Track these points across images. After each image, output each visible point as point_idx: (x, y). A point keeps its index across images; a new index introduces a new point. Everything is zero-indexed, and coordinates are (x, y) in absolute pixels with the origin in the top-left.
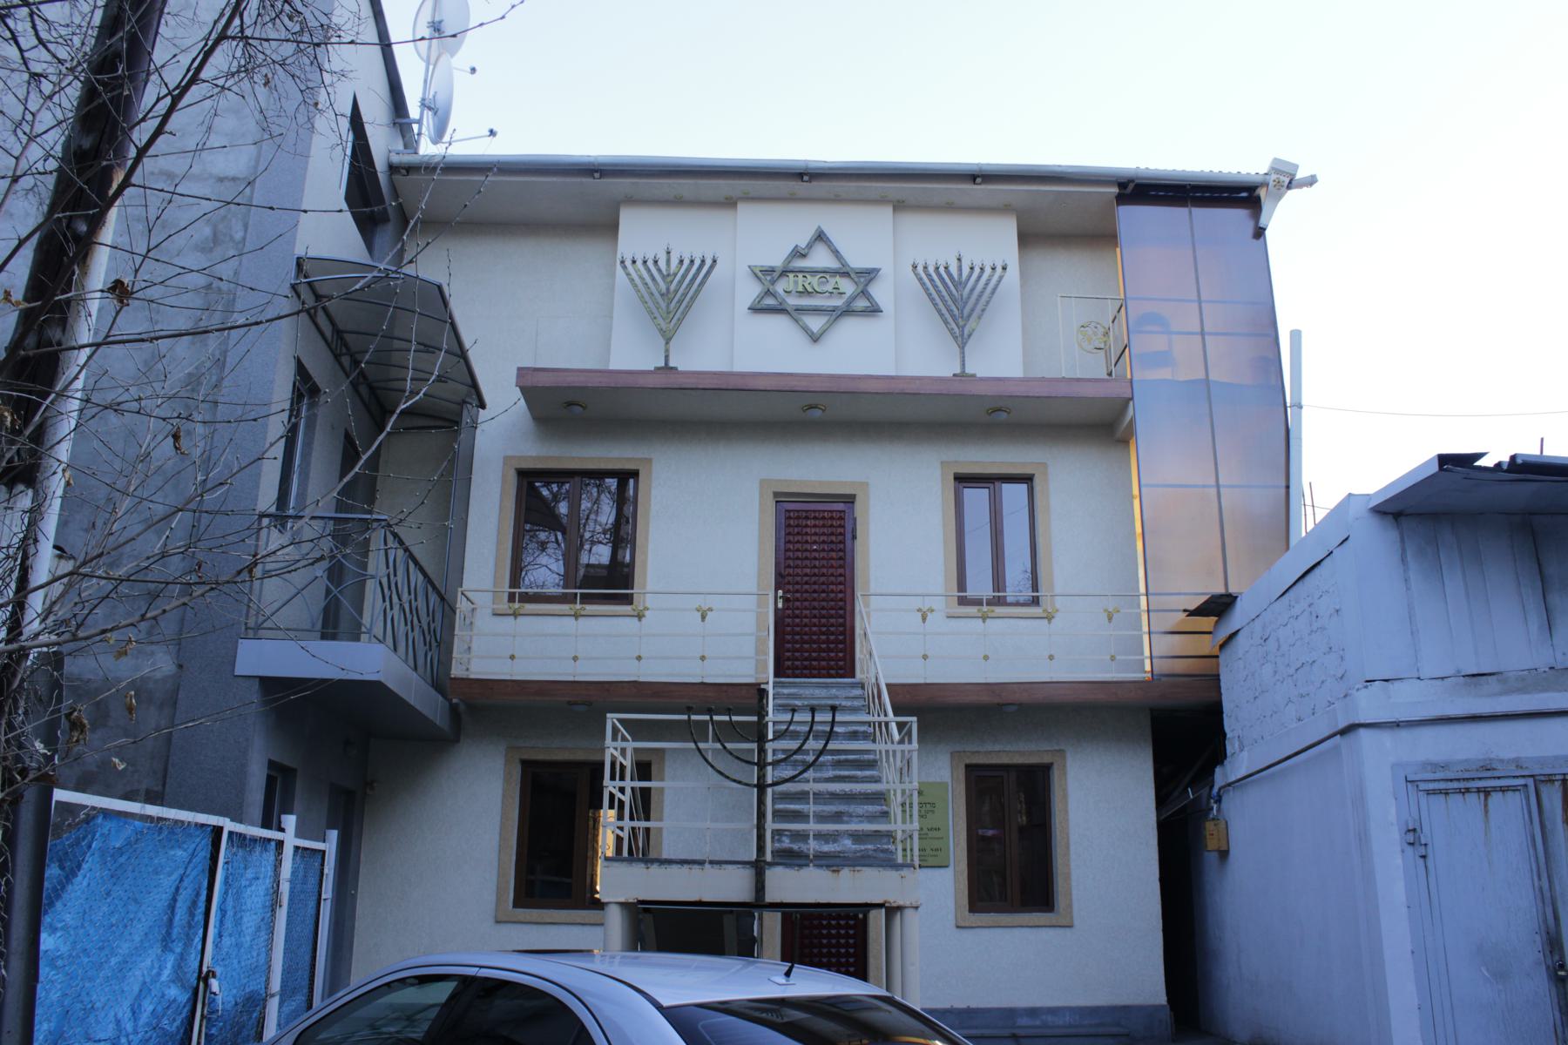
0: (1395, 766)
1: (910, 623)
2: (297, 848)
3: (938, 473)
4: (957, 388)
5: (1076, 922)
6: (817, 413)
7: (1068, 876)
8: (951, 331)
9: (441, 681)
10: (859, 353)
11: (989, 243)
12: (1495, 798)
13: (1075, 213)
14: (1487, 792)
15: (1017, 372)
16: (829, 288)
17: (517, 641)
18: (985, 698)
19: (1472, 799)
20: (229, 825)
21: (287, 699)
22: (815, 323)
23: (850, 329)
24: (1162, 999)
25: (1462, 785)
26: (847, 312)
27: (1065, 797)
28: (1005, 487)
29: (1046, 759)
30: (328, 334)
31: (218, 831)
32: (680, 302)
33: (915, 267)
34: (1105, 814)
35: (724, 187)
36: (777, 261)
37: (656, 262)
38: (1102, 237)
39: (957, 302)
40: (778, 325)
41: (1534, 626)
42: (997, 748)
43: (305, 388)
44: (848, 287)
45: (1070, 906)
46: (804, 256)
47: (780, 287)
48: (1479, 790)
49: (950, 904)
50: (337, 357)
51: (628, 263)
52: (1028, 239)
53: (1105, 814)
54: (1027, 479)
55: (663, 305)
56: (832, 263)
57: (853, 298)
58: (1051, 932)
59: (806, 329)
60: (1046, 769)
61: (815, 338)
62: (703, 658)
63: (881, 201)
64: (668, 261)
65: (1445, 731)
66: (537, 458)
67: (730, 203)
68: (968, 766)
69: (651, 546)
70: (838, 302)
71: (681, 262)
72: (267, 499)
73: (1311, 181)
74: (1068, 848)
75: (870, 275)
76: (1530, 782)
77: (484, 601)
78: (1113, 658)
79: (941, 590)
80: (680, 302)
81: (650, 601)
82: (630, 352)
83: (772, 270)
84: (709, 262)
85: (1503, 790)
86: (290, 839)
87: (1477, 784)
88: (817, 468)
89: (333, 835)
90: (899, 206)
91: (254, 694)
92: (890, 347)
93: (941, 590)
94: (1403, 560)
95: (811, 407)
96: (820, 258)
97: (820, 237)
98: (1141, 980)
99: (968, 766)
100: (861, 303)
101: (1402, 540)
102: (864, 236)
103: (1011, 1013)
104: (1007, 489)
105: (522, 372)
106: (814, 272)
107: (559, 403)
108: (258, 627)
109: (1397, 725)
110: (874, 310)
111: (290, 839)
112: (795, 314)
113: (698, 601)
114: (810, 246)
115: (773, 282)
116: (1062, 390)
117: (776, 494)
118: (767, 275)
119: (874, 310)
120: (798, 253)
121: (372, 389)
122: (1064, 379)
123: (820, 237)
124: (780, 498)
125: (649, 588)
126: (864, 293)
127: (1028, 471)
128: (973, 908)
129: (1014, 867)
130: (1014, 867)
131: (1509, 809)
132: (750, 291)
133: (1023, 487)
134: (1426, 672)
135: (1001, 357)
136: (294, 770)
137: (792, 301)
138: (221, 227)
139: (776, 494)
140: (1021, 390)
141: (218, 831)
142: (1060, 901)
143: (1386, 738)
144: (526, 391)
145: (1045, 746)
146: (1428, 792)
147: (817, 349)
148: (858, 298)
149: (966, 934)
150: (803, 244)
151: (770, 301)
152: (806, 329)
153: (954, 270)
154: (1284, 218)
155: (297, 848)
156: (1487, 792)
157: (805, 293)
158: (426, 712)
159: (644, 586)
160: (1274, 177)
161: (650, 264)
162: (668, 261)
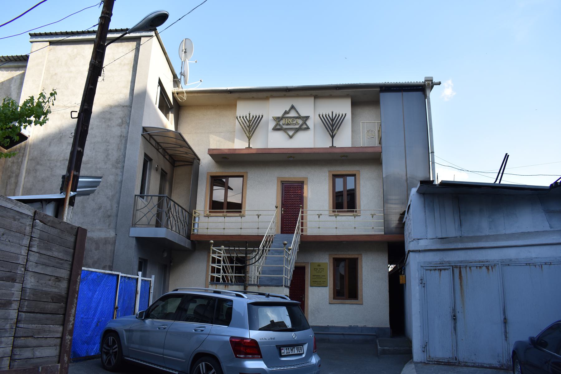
3: (328, 174)
4: (330, 151)
5: (364, 303)
6: (291, 159)
7: (362, 290)
8: (330, 134)
9: (188, 236)
11: (343, 108)
12: (443, 272)
13: (365, 97)
14: (440, 270)
15: (350, 145)
16: (295, 122)
17: (209, 224)
19: (437, 272)
20: (121, 274)
21: (142, 242)
22: (291, 133)
24: (388, 325)
25: (435, 268)
26: (297, 130)
28: (348, 178)
29: (356, 256)
31: (118, 275)
32: (253, 128)
33: (319, 115)
35: (265, 94)
36: (280, 115)
37: (246, 117)
39: (332, 125)
41: (457, 226)
42: (343, 253)
43: (147, 160)
44: (300, 122)
45: (362, 299)
46: (288, 113)
47: (281, 123)
48: (439, 269)
49: (328, 297)
50: (158, 150)
51: (238, 118)
52: (354, 104)
53: (373, 274)
54: (354, 175)
55: (248, 129)
56: (296, 115)
57: (302, 125)
59: (288, 135)
60: (357, 259)
61: (291, 137)
63: (310, 96)
65: (431, 254)
66: (216, 172)
67: (267, 98)
68: (334, 258)
69: (247, 197)
70: (297, 127)
71: (253, 117)
72: (138, 192)
73: (439, 84)
74: (362, 281)
75: (307, 118)
76: (451, 267)
77: (202, 213)
78: (373, 228)
79: (327, 209)
80: (253, 128)
81: (247, 213)
82: (239, 144)
83: (279, 118)
84: (261, 117)
85: (445, 269)
86: (140, 278)
87: (439, 268)
88: (293, 174)
91: (134, 242)
92: (310, 140)
93: (327, 209)
94: (425, 207)
96: (293, 114)
97: (293, 107)
99: (334, 258)
100: (305, 126)
102: (305, 107)
103: (327, 328)
105: (209, 150)
106: (290, 118)
108: (135, 224)
109: (419, 251)
110: (308, 128)
111: (140, 278)
112: (285, 130)
113: (257, 213)
114: (290, 110)
115: (279, 121)
117: (281, 181)
118: (278, 119)
119: (308, 128)
120: (286, 112)
122: (361, 147)
123: (293, 107)
125: (246, 209)
127: (354, 173)
128: (334, 298)
129: (347, 288)
130: (347, 288)
132: (272, 125)
133: (353, 178)
135: (344, 140)
136: (147, 260)
137: (285, 127)
139: (281, 181)
140: (349, 151)
142: (359, 297)
143: (417, 255)
144: (211, 155)
146: (427, 270)
147: (292, 140)
148: (302, 125)
149: (333, 306)
150: (288, 110)
151: (278, 127)
152: (288, 135)
153: (331, 116)
154: (433, 95)
155: (142, 280)
156: (440, 270)
157: (288, 124)
158: (182, 244)
159: (245, 208)
160: (426, 83)
161: (244, 118)
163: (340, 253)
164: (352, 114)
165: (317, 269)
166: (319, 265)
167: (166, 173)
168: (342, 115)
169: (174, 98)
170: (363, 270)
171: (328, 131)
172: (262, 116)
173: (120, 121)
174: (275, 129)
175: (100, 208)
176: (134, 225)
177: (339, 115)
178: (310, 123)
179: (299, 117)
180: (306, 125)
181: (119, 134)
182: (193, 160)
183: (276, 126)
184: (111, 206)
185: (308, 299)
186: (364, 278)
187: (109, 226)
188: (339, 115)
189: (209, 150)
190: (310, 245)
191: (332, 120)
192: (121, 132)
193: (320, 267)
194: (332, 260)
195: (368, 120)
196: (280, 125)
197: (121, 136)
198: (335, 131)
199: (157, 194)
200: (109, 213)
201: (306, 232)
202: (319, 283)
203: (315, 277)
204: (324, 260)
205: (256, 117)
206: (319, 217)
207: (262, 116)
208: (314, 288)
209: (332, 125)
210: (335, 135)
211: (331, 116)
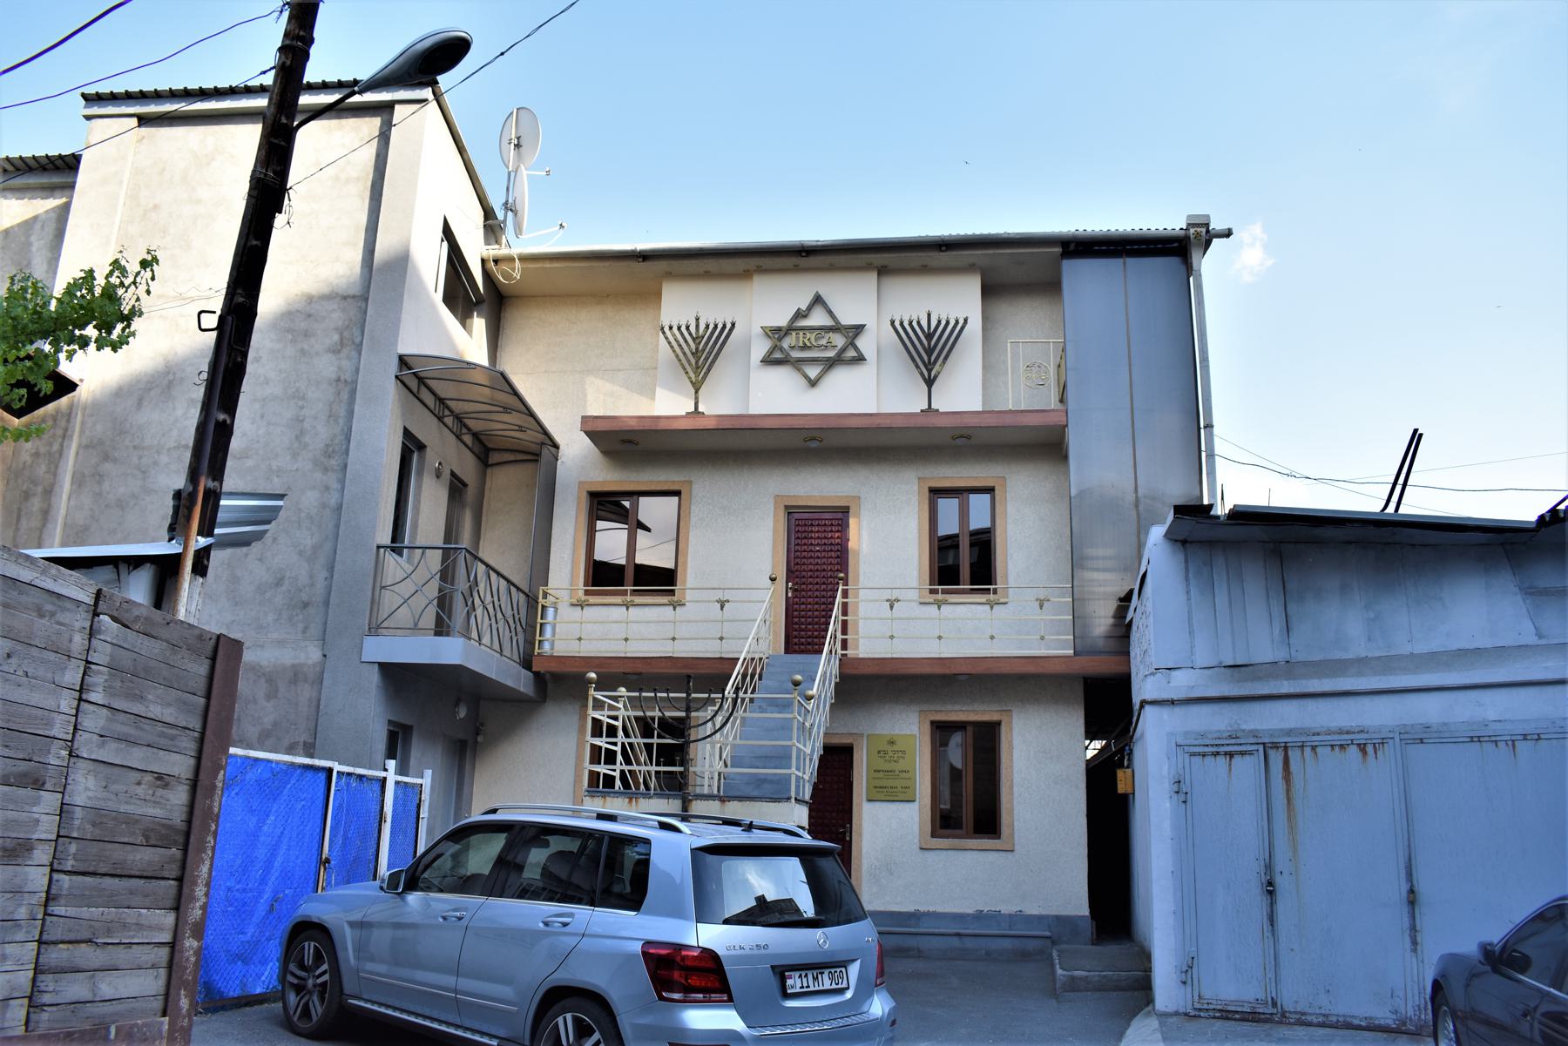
0: (1170, 734)
1: (892, 608)
2: (397, 783)
3: (916, 488)
5: (1017, 848)
6: (814, 444)
10: (850, 395)
11: (956, 300)
12: (1237, 759)
13: (1020, 270)
14: (1231, 755)
15: (977, 406)
16: (824, 342)
17: (583, 628)
19: (1221, 760)
21: (396, 676)
22: (813, 372)
23: (841, 378)
24: (1084, 910)
25: (1215, 749)
26: (830, 364)
31: (330, 770)
32: (707, 359)
33: (893, 323)
34: (1044, 760)
36: (783, 322)
37: (687, 328)
38: (1051, 287)
39: (928, 350)
40: (782, 374)
44: (839, 340)
45: (1012, 835)
46: (805, 316)
47: (786, 344)
48: (1226, 754)
50: (440, 419)
51: (666, 329)
52: (990, 291)
53: (1044, 760)
54: (990, 490)
55: (693, 361)
56: (829, 322)
57: (843, 350)
58: (995, 854)
59: (806, 377)
60: (999, 723)
61: (813, 383)
63: (867, 268)
64: (697, 326)
65: (1205, 709)
66: (604, 482)
68: (932, 723)
69: (690, 550)
70: (831, 354)
72: (385, 537)
73: (1228, 234)
75: (859, 329)
76: (1261, 748)
77: (564, 596)
78: (1042, 638)
79: (915, 584)
80: (707, 359)
81: (689, 595)
82: (669, 403)
83: (779, 329)
84: (729, 326)
85: (1242, 753)
86: (392, 777)
87: (1227, 750)
88: (818, 486)
89: (428, 773)
90: (883, 271)
92: (868, 391)
94: (1187, 579)
96: (818, 319)
97: (818, 300)
98: (1067, 890)
99: (932, 723)
100: (851, 353)
101: (1186, 561)
102: (854, 300)
104: (974, 499)
105: (585, 419)
107: (618, 441)
108: (378, 627)
109: (1173, 702)
110: (860, 359)
112: (797, 364)
113: (719, 595)
114: (810, 308)
115: (780, 339)
116: (1009, 421)
117: (786, 507)
118: (777, 334)
119: (860, 359)
120: (800, 315)
121: (475, 435)
122: (1010, 411)
123: (818, 300)
124: (790, 511)
126: (853, 344)
132: (760, 348)
134: (1199, 664)
135: (962, 392)
137: (796, 354)
139: (786, 507)
141: (330, 770)
142: (1005, 830)
143: (1165, 713)
144: (589, 434)
145: (995, 707)
146: (1193, 754)
147: (816, 392)
148: (844, 349)
149: (930, 855)
150: (804, 308)
151: (778, 355)
152: (806, 377)
153: (924, 323)
154: (1211, 264)
155: (397, 783)
156: (1231, 755)
157: (804, 348)
158: (510, 683)
159: (857, 633)
160: (1192, 231)
161: (683, 329)
162: (697, 326)
164: (985, 318)
165: (886, 753)
166: (892, 743)
167: (465, 485)
168: (957, 322)
169: (487, 274)
171: (917, 366)
172: (733, 325)
173: (336, 337)
174: (769, 361)
175: (279, 582)
176: (375, 629)
177: (948, 323)
178: (865, 344)
179: (837, 328)
180: (856, 349)
181: (334, 376)
182: (537, 450)
183: (771, 352)
184: (311, 577)
185: (860, 835)
186: (1017, 780)
188: (948, 323)
189: (585, 419)
190: (865, 685)
191: (929, 336)
192: (340, 368)
193: (895, 748)
194: (927, 728)
195: (1030, 329)
196: (781, 349)
197: (338, 380)
198: (937, 367)
200: (304, 597)
201: (857, 648)
202: (892, 791)
204: (906, 728)
205: (716, 326)
206: (892, 608)
207: (733, 325)
208: (878, 804)
209: (928, 350)
211: (924, 323)
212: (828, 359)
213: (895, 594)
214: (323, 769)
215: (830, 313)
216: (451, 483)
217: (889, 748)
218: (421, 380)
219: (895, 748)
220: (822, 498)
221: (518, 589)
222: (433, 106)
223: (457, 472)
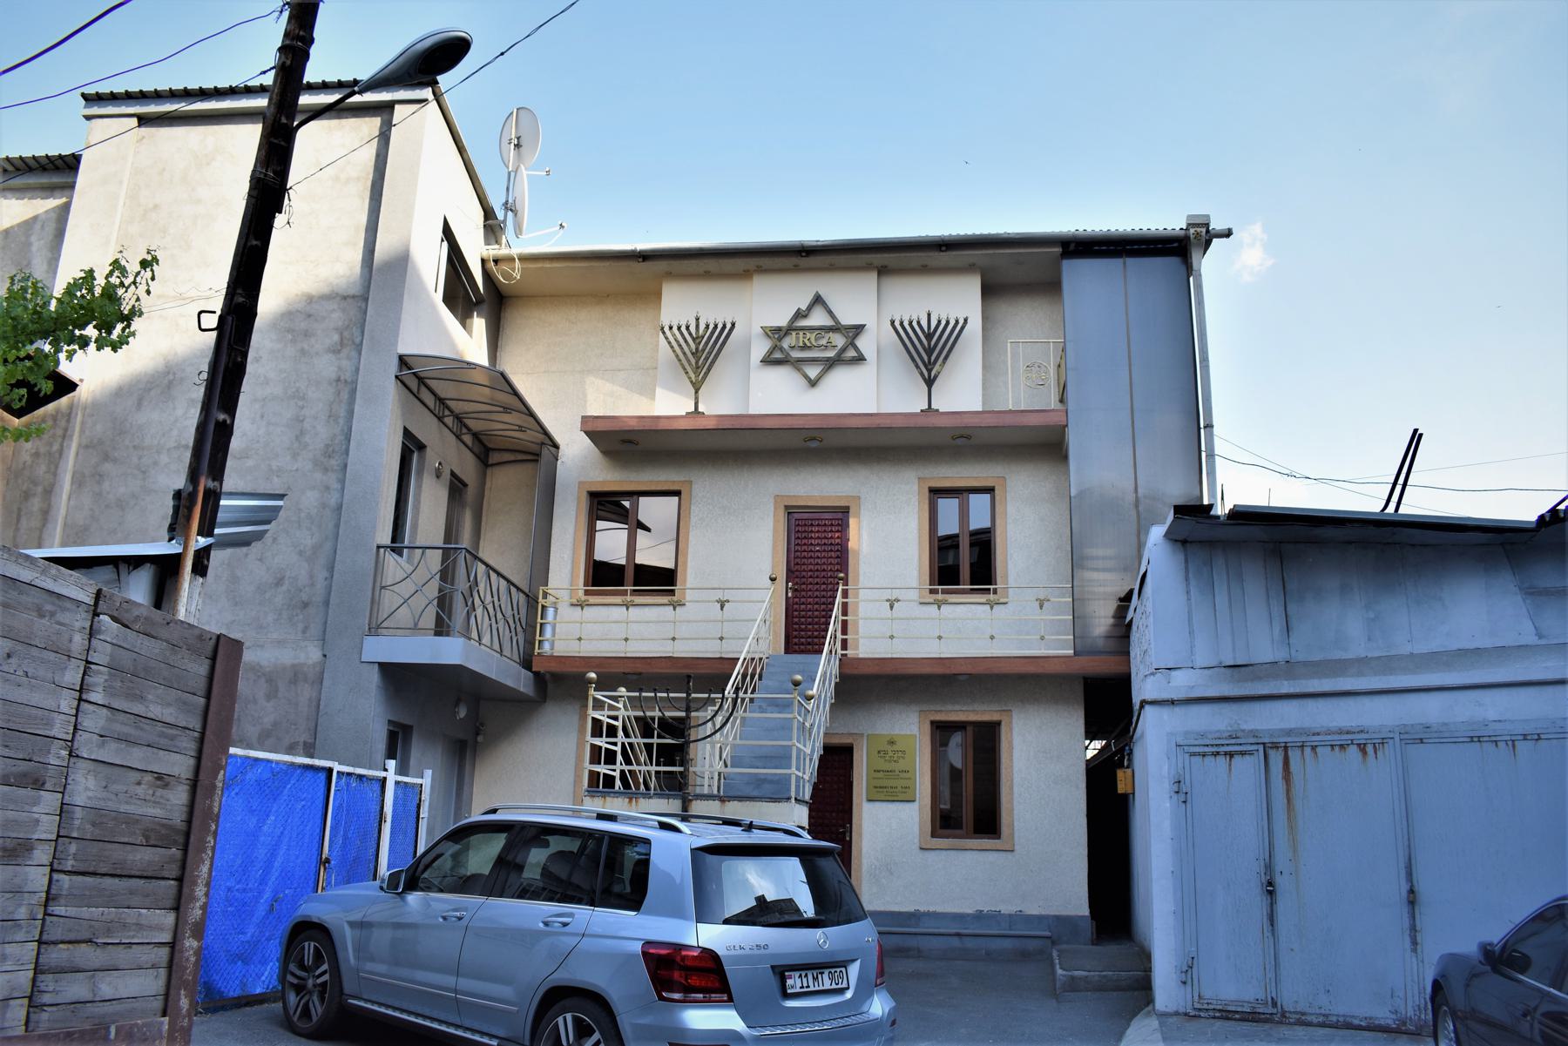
1: (892, 608)
2: (397, 783)
3: (916, 487)
6: (814, 444)
8: (922, 374)
10: (851, 395)
11: (956, 300)
12: (1237, 759)
13: (1020, 270)
14: (1231, 755)
15: (977, 406)
16: (823, 342)
17: (583, 628)
18: (939, 670)
19: (1221, 760)
21: (396, 676)
22: (813, 372)
23: (841, 378)
24: (1084, 910)
25: (1215, 749)
26: (830, 364)
27: (1011, 747)
30: (431, 405)
32: (707, 359)
33: (893, 323)
34: (1044, 760)
36: (782, 321)
37: (687, 328)
38: (1050, 287)
39: (928, 350)
40: (782, 374)
44: (839, 340)
46: (805, 316)
47: (786, 344)
48: (1225, 754)
51: (666, 329)
52: (990, 291)
53: (1044, 760)
54: (990, 490)
55: (693, 361)
57: (844, 350)
59: (806, 377)
60: (998, 724)
61: (813, 383)
62: (721, 639)
63: (867, 268)
65: (1205, 709)
66: (604, 482)
68: (932, 723)
69: (690, 550)
70: (831, 354)
72: (385, 537)
73: (1228, 234)
75: (859, 329)
76: (1261, 748)
77: (564, 596)
78: (1042, 638)
79: (915, 584)
80: (707, 359)
81: (689, 595)
82: (669, 403)
83: (779, 329)
84: (729, 326)
85: (1243, 753)
86: (392, 777)
87: (1227, 750)
88: (818, 486)
90: (883, 271)
91: (374, 676)
92: (868, 391)
94: (1187, 579)
95: (814, 439)
96: (818, 319)
97: (818, 300)
98: (1066, 890)
99: (932, 723)
100: (851, 353)
101: (1186, 561)
102: (853, 300)
104: (974, 499)
105: (585, 419)
106: (812, 329)
107: (618, 441)
108: (378, 627)
109: (1173, 702)
110: (860, 359)
112: (797, 364)
113: (719, 595)
114: (810, 308)
115: (780, 339)
116: (1009, 421)
117: (786, 507)
118: (777, 334)
119: (860, 359)
120: (800, 315)
122: (1011, 411)
123: (818, 300)
124: (790, 511)
131: (1247, 768)
132: (760, 348)
134: (1199, 664)
135: (962, 392)
137: (796, 354)
138: (346, 334)
139: (786, 507)
140: (975, 421)
142: (1005, 830)
143: (1165, 713)
144: (589, 434)
146: (1193, 754)
147: (816, 392)
148: (844, 348)
149: (931, 855)
150: (804, 308)
151: (778, 355)
152: (806, 377)
153: (924, 323)
154: (1211, 265)
155: (397, 783)
156: (1231, 755)
157: (804, 348)
159: (857, 633)
161: (683, 329)
163: (950, 707)
164: (985, 318)
165: (886, 753)
166: (892, 743)
167: (465, 485)
169: (487, 274)
170: (1016, 754)
171: (917, 366)
172: (733, 325)
173: (336, 337)
174: (768, 361)
175: (279, 582)
176: (375, 629)
177: (948, 323)
178: (865, 344)
179: (837, 328)
181: (334, 376)
182: (537, 450)
183: (771, 352)
184: (311, 577)
186: (1016, 780)
187: (304, 632)
188: (948, 323)
189: (585, 419)
190: (865, 685)
191: (929, 336)
193: (895, 748)
194: (927, 728)
195: (1028, 325)
196: (781, 349)
197: (338, 380)
198: (937, 368)
199: (440, 543)
200: (304, 597)
201: (857, 648)
202: (891, 791)
203: (881, 775)
204: (906, 728)
205: (716, 326)
206: (892, 608)
207: (733, 325)
208: (878, 804)
209: (928, 350)
210: (936, 377)
211: (924, 323)
212: (828, 359)
213: (895, 594)
214: (323, 769)
215: (830, 313)
216: (451, 483)
217: (889, 748)
218: (421, 380)
219: (895, 748)
220: (822, 498)
221: (518, 589)
222: (433, 106)
223: (457, 472)
